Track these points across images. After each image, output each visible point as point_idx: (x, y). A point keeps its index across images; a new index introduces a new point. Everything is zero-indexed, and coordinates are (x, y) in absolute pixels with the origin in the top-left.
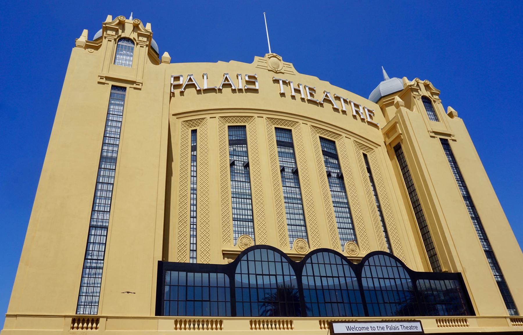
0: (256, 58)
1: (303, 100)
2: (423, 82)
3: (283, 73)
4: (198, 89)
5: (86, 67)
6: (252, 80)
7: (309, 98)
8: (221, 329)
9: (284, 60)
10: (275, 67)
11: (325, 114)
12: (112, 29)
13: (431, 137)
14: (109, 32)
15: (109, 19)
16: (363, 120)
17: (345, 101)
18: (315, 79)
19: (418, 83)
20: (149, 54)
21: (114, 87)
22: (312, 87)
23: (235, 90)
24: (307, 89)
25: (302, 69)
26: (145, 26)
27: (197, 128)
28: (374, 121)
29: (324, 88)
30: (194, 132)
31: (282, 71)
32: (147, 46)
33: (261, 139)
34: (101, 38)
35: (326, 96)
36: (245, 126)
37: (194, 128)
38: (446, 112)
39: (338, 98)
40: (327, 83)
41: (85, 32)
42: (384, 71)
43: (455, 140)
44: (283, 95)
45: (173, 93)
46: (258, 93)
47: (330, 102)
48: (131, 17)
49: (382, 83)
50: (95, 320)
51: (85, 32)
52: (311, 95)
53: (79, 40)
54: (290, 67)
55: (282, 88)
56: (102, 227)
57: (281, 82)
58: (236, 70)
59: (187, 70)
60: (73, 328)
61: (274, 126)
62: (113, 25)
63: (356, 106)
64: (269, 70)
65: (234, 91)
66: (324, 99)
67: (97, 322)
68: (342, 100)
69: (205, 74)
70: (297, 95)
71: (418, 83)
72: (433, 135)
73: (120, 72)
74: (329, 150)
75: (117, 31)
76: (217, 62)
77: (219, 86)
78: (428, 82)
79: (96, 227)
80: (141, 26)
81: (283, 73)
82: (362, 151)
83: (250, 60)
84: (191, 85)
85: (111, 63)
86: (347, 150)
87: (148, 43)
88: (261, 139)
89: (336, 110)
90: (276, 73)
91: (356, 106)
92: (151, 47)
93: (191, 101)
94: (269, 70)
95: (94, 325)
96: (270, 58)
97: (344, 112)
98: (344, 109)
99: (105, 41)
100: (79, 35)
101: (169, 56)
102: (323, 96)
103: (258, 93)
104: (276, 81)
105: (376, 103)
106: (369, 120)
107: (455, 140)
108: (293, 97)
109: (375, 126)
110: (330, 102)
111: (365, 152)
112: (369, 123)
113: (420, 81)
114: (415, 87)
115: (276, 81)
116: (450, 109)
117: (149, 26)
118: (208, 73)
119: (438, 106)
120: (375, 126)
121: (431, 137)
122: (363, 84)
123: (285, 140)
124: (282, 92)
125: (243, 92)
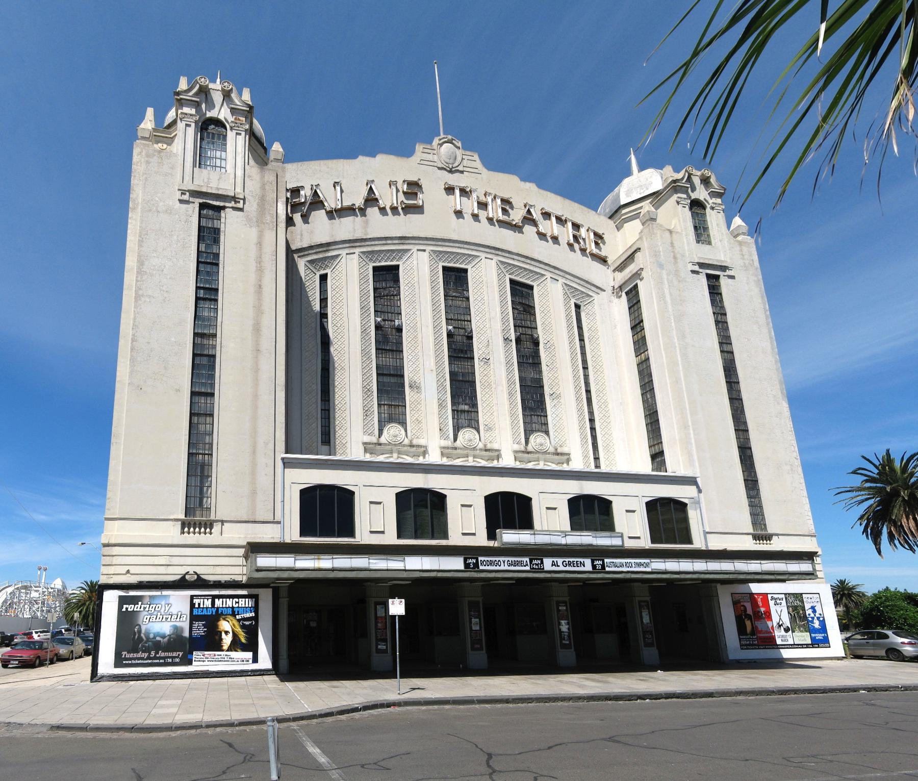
0: (419, 148)
1: (490, 220)
2: (699, 173)
3: (462, 172)
4: (328, 209)
5: (162, 175)
6: (414, 188)
7: (501, 216)
8: (211, 533)
9: (465, 148)
10: (448, 161)
11: (526, 242)
12: (190, 103)
13: (693, 272)
14: (186, 110)
15: (183, 85)
16: (583, 251)
17: (559, 220)
18: (514, 180)
19: (690, 175)
20: (251, 148)
21: (202, 206)
22: (506, 196)
23: (384, 208)
24: (499, 201)
25: (494, 164)
26: (240, 94)
27: (328, 271)
28: (603, 253)
29: (526, 195)
30: (324, 278)
31: (460, 168)
32: (246, 131)
33: (420, 281)
34: (174, 123)
35: (529, 212)
36: (397, 267)
37: (323, 272)
38: (729, 227)
39: (547, 215)
40: (531, 186)
41: (150, 112)
42: (633, 157)
43: (732, 277)
44: (459, 214)
45: (291, 219)
46: (422, 213)
47: (534, 223)
48: (218, 80)
49: (626, 181)
50: (208, 523)
51: (150, 112)
52: (504, 211)
53: (142, 126)
54: (473, 161)
55: (457, 200)
56: (206, 415)
57: (457, 192)
58: (383, 172)
59: (307, 175)
60: (183, 533)
61: (441, 264)
62: (189, 96)
63: (576, 226)
64: (439, 168)
65: (383, 210)
66: (525, 218)
67: (211, 527)
68: (553, 219)
69: (337, 183)
70: (483, 215)
71: (690, 175)
72: (696, 268)
73: (209, 181)
74: (521, 296)
75: (197, 105)
76: (355, 157)
77: (359, 202)
78: (707, 173)
79: (198, 415)
80: (234, 95)
81: (462, 172)
82: (573, 301)
83: (407, 153)
84: (317, 202)
85: (194, 166)
86: (550, 302)
87: (247, 127)
88: (420, 281)
89: (542, 236)
90: (451, 171)
91: (576, 226)
92: (252, 134)
93: (319, 229)
94: (439, 168)
95: (208, 530)
96: (441, 145)
97: (555, 239)
98: (556, 233)
99: (181, 125)
100: (142, 118)
101: (281, 150)
102: (522, 212)
103: (422, 213)
104: (450, 190)
105: (610, 218)
106: (595, 251)
107: (732, 277)
108: (475, 217)
109: (603, 260)
110: (534, 223)
111: (578, 302)
112: (594, 257)
113: (695, 172)
114: (683, 183)
115: (450, 190)
116: (737, 221)
117: (246, 96)
118: (341, 178)
119: (714, 219)
120: (603, 260)
121: (693, 272)
122: (590, 183)
123: (455, 279)
124: (458, 208)
125: (399, 214)
